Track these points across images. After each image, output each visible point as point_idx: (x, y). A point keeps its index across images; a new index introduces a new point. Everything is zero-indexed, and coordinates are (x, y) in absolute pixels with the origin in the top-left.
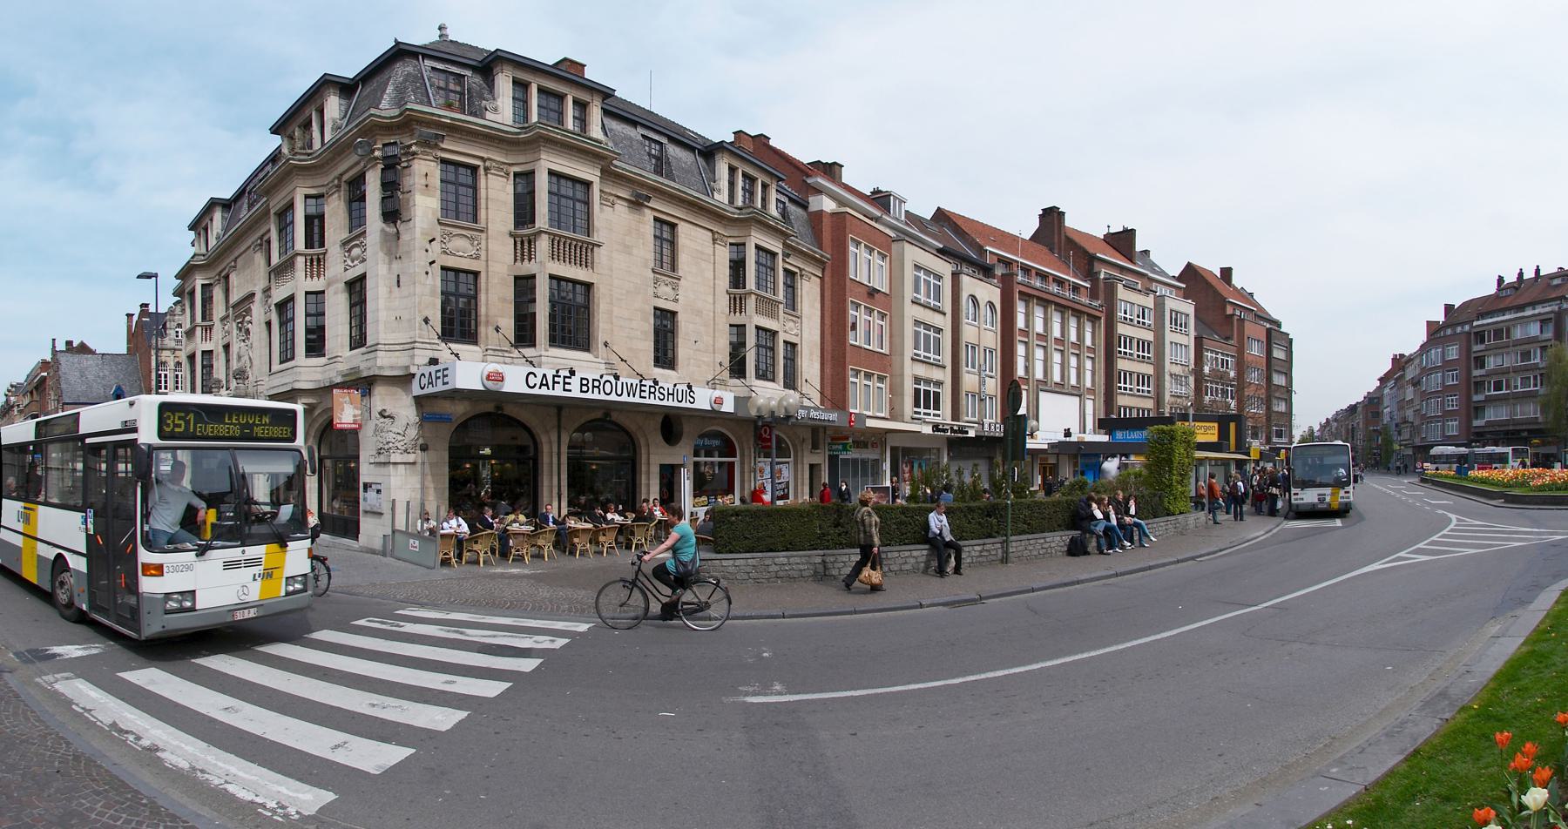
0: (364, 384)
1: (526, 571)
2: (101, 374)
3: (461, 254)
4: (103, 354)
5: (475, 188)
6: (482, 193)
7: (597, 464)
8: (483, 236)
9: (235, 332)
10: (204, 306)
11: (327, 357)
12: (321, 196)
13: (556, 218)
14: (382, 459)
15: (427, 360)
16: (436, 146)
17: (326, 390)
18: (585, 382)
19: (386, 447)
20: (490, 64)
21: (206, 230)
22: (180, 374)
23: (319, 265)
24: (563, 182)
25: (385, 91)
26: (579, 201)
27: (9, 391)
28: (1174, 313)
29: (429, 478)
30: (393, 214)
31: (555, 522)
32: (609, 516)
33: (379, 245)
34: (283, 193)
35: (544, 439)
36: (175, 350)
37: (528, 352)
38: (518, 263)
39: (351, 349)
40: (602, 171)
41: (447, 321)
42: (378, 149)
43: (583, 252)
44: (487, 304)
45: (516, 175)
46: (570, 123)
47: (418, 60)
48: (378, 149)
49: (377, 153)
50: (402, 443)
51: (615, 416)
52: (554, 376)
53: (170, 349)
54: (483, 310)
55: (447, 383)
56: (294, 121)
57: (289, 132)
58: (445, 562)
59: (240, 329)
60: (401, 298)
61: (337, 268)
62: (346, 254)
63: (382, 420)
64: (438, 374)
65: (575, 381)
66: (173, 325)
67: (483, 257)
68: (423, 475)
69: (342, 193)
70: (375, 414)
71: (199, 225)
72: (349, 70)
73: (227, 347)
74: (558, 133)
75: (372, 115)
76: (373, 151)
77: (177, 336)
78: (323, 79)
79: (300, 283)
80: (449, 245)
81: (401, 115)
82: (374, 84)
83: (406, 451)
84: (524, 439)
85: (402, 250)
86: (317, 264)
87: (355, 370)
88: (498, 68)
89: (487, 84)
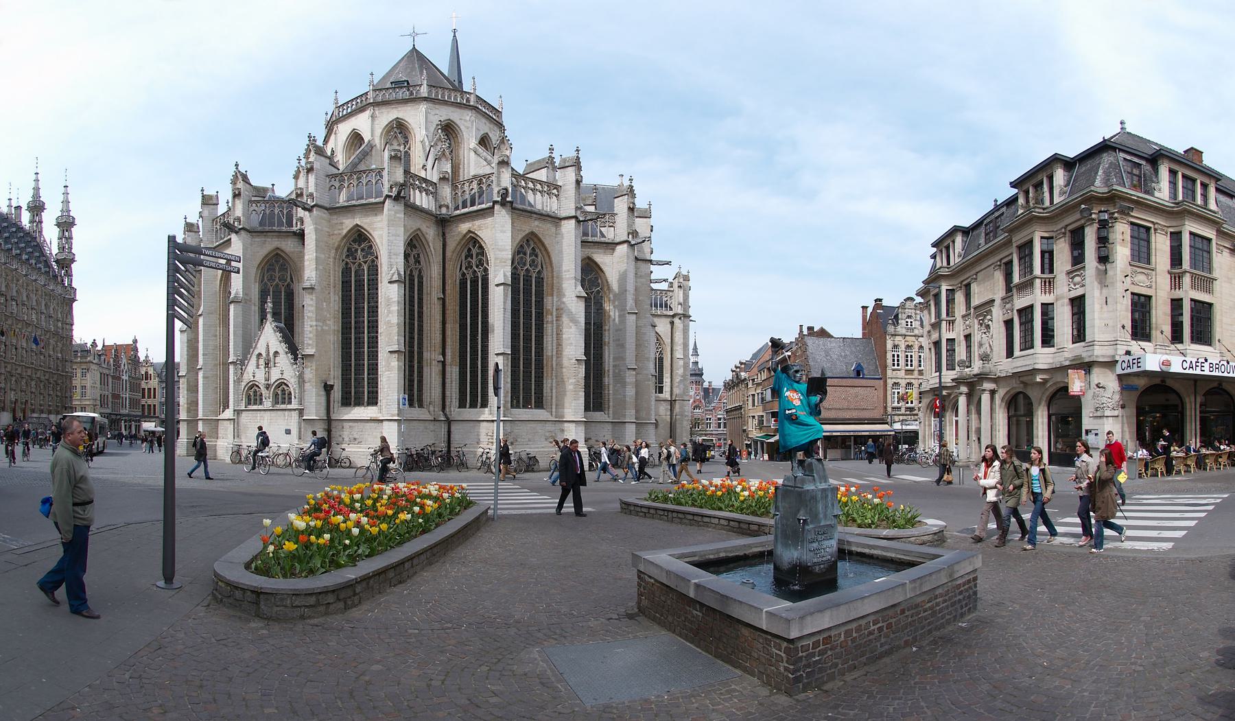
0: (1086, 367)
1: (1184, 478)
2: (843, 354)
3: (1142, 284)
4: (844, 338)
5: (1148, 242)
6: (1153, 245)
7: (1213, 415)
8: (1154, 272)
9: (976, 326)
10: (947, 306)
11: (1056, 348)
12: (1052, 238)
13: (1194, 265)
14: (1099, 414)
15: (1125, 352)
16: (1128, 214)
17: (1063, 369)
18: (1211, 365)
19: (1102, 406)
20: (1157, 156)
21: (948, 248)
22: (922, 354)
23: (1050, 285)
24: (1197, 238)
25: (1097, 173)
26: (1205, 251)
27: (736, 367)
28: (103, 375)
29: (1126, 425)
30: (1104, 259)
31: (1194, 451)
32: (1222, 447)
33: (1094, 277)
34: (1025, 233)
35: (1187, 400)
36: (906, 336)
37: (1179, 346)
38: (1173, 290)
39: (1073, 343)
40: (1217, 232)
41: (1134, 327)
42: (1095, 213)
43: (1206, 283)
44: (1156, 317)
45: (1171, 233)
46: (1199, 201)
47: (1116, 152)
48: (1095, 213)
49: (1093, 216)
50: (1111, 404)
51: (1225, 386)
52: (1196, 362)
53: (901, 335)
54: (1154, 320)
55: (1204, 371)
56: (1032, 180)
57: (1025, 188)
58: (1140, 475)
59: (981, 325)
60: (1108, 311)
61: (1063, 290)
62: (1070, 280)
63: (1098, 389)
64: (1134, 361)
65: (1206, 365)
66: (904, 316)
67: (1154, 287)
68: (1123, 423)
69: (1067, 238)
70: (1093, 385)
71: (943, 244)
72: (1071, 152)
73: (968, 337)
74: (1195, 208)
75: (1092, 191)
76: (1091, 215)
77: (907, 325)
78: (1054, 157)
79: (1037, 297)
80: (1135, 279)
81: (1109, 192)
82: (1089, 164)
83: (1113, 409)
84: (1173, 399)
85: (1108, 281)
86: (1049, 284)
87: (1078, 357)
88: (1161, 161)
89: (1154, 171)
